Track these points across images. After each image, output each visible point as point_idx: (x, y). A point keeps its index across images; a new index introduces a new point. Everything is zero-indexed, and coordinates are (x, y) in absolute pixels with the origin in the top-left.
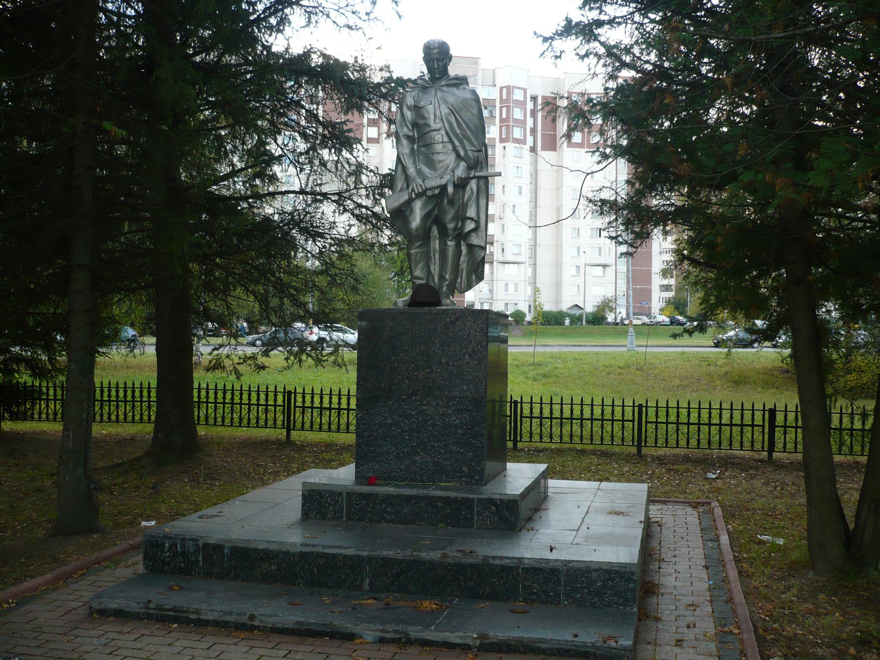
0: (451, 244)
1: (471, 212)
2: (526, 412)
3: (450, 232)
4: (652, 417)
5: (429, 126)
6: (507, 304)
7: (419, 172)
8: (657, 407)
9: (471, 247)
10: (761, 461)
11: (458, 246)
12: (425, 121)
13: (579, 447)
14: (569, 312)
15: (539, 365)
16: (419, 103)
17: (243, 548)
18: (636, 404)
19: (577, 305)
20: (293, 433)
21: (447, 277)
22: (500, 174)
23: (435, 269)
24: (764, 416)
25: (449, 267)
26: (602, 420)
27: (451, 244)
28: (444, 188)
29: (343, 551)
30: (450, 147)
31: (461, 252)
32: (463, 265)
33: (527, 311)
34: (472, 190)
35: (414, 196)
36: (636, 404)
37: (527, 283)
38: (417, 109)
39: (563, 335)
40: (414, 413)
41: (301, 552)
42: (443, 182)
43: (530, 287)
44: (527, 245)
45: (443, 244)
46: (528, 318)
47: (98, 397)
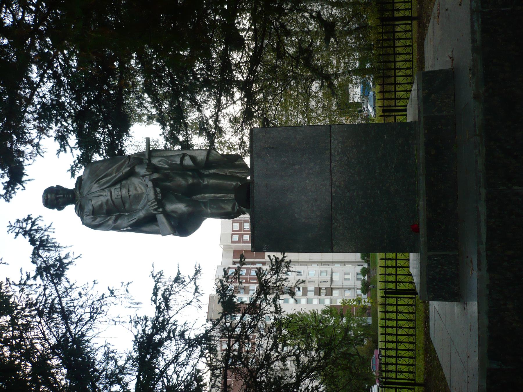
3: (195, 181)
5: (108, 200)
6: (357, 279)
10: (419, 25)
12: (104, 204)
16: (90, 210)
18: (382, 114)
21: (234, 183)
22: (148, 140)
28: (156, 183)
29: (483, 218)
30: (124, 182)
31: (214, 174)
33: (361, 267)
34: (159, 161)
35: (161, 210)
37: (344, 267)
38: (95, 213)
40: (348, 194)
41: (489, 270)
42: (150, 184)
43: (347, 265)
44: (321, 267)
46: (366, 266)
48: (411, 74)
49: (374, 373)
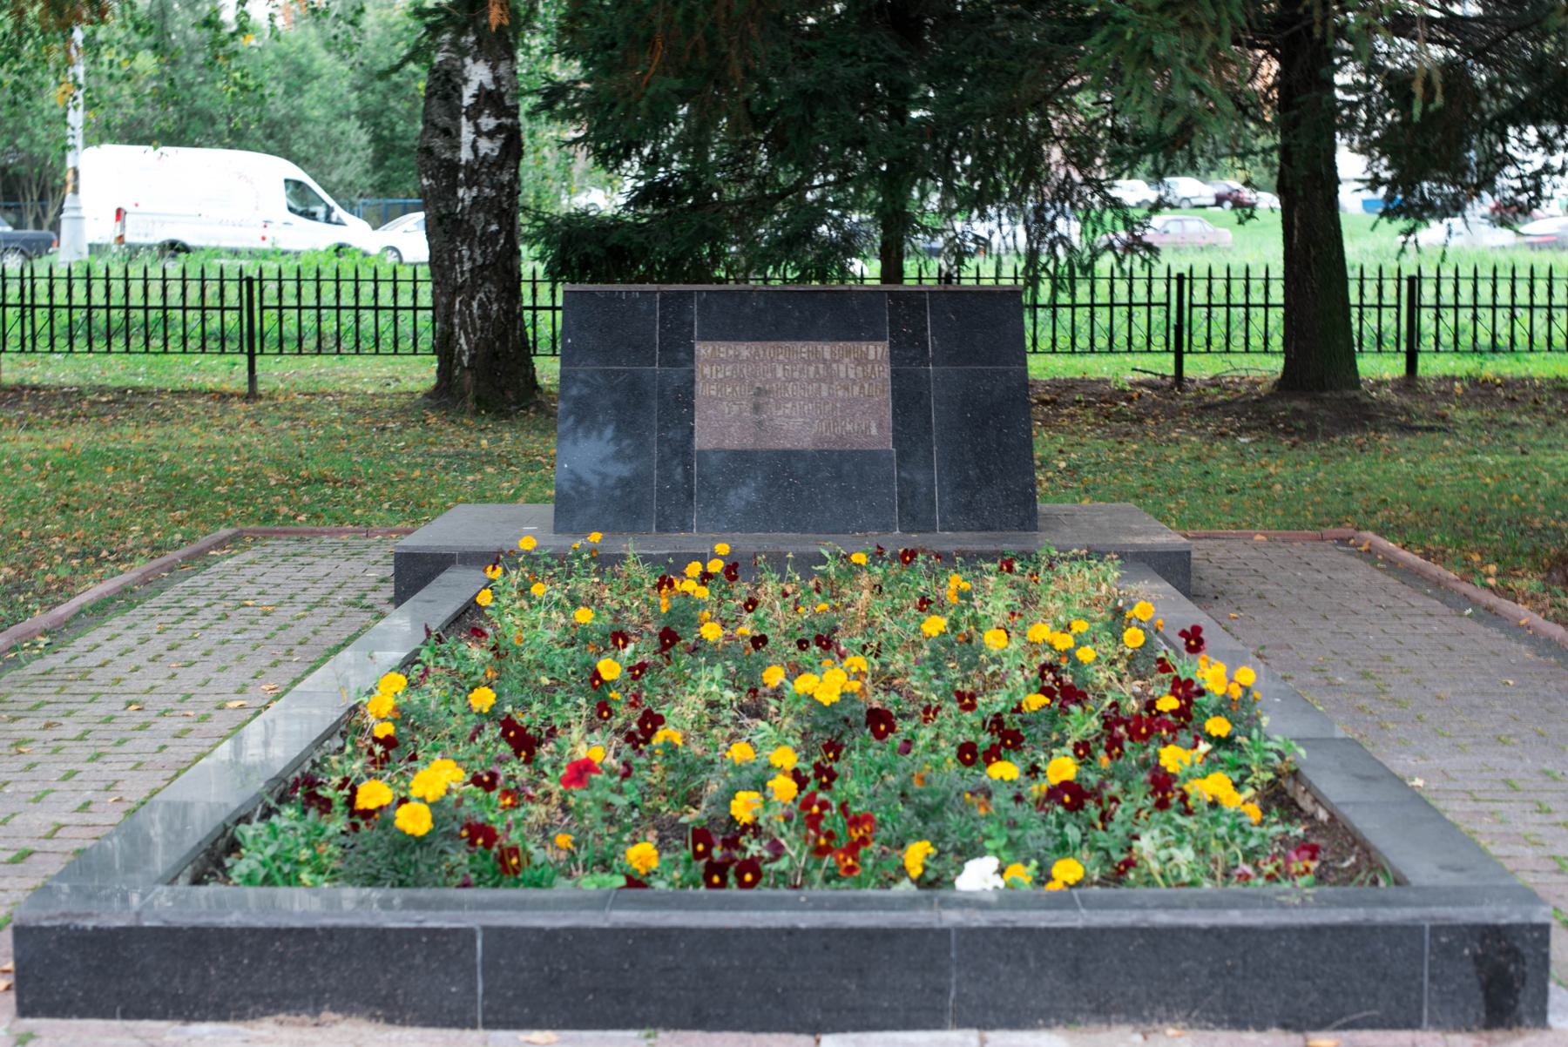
4: (1200, 296)
8: (51, 278)
17: (70, 1017)
18: (1173, 274)
20: (1187, 359)
24: (1168, 286)
26: (1130, 305)
36: (1173, 274)
47: (1354, 298)
48: (1115, 348)
49: (855, 217)
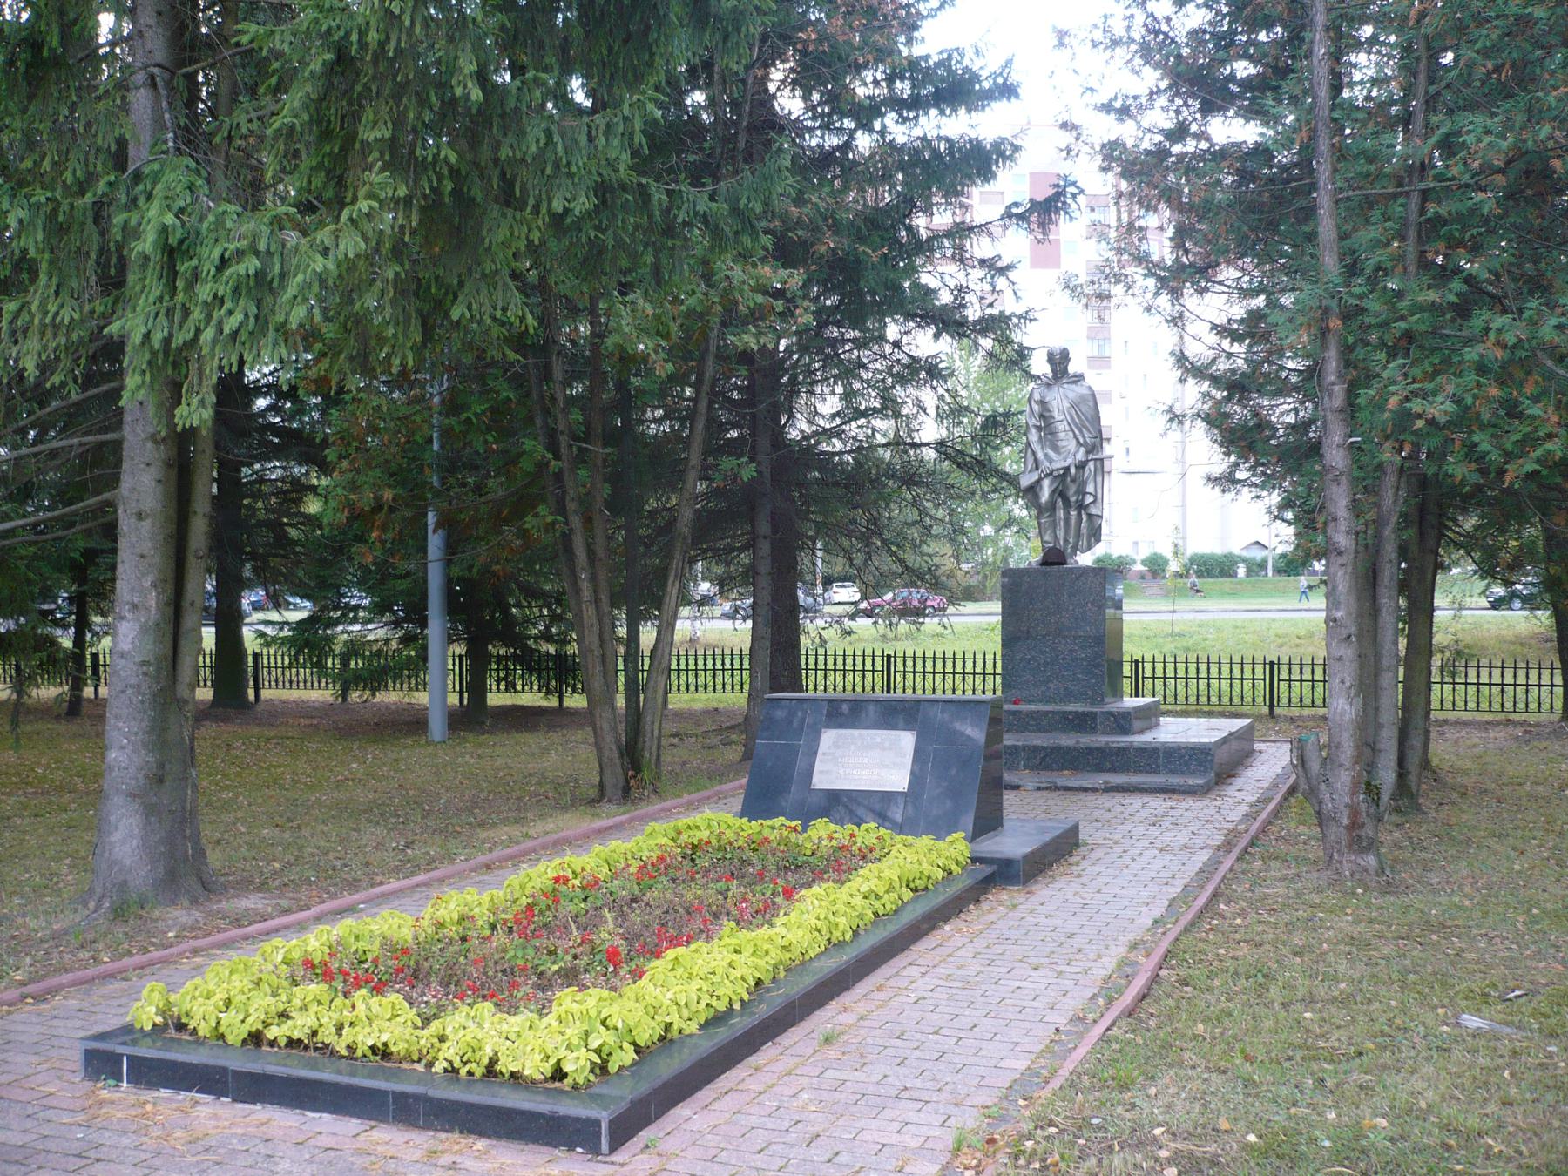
0: (1073, 513)
1: (1090, 488)
2: (1148, 673)
7: (1046, 455)
9: (1090, 516)
11: (1079, 515)
13: (1206, 708)
14: (1245, 554)
15: (1179, 635)
19: (1258, 543)
23: (1061, 534)
25: (1072, 532)
27: (1073, 513)
28: (1067, 469)
32: (1084, 531)
38: (1043, 403)
39: (1233, 594)
45: (1067, 514)
46: (1174, 566)
